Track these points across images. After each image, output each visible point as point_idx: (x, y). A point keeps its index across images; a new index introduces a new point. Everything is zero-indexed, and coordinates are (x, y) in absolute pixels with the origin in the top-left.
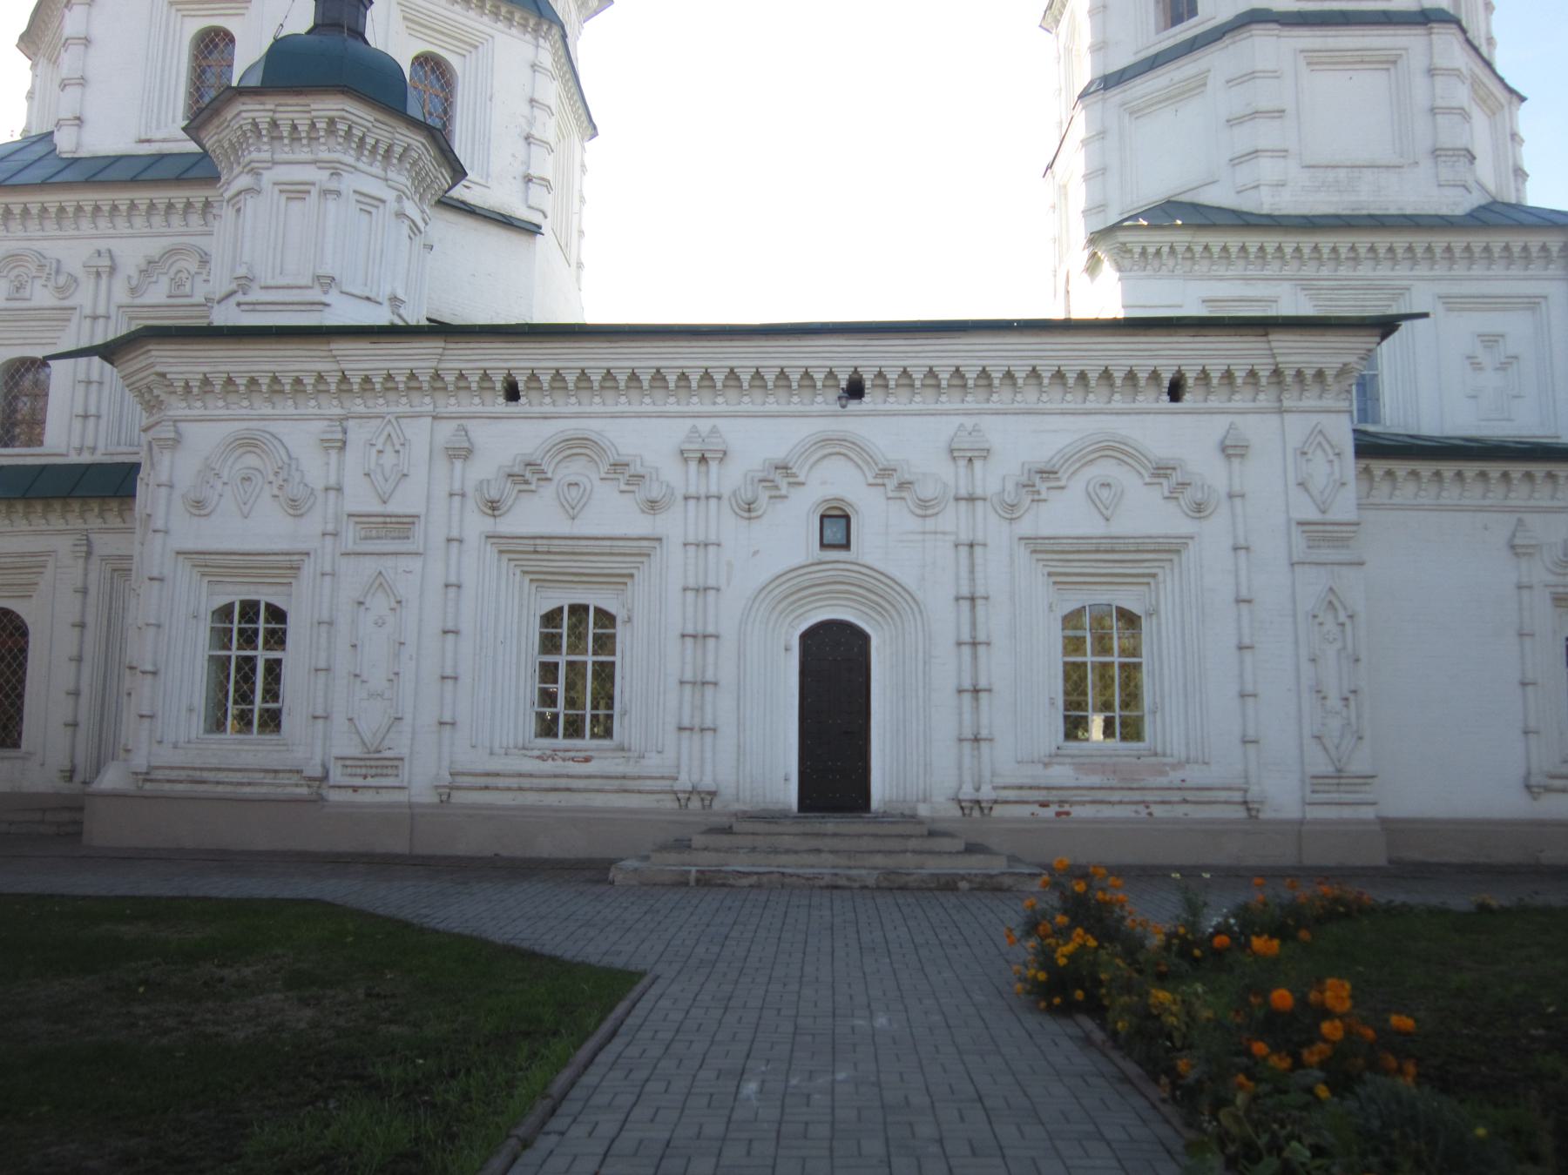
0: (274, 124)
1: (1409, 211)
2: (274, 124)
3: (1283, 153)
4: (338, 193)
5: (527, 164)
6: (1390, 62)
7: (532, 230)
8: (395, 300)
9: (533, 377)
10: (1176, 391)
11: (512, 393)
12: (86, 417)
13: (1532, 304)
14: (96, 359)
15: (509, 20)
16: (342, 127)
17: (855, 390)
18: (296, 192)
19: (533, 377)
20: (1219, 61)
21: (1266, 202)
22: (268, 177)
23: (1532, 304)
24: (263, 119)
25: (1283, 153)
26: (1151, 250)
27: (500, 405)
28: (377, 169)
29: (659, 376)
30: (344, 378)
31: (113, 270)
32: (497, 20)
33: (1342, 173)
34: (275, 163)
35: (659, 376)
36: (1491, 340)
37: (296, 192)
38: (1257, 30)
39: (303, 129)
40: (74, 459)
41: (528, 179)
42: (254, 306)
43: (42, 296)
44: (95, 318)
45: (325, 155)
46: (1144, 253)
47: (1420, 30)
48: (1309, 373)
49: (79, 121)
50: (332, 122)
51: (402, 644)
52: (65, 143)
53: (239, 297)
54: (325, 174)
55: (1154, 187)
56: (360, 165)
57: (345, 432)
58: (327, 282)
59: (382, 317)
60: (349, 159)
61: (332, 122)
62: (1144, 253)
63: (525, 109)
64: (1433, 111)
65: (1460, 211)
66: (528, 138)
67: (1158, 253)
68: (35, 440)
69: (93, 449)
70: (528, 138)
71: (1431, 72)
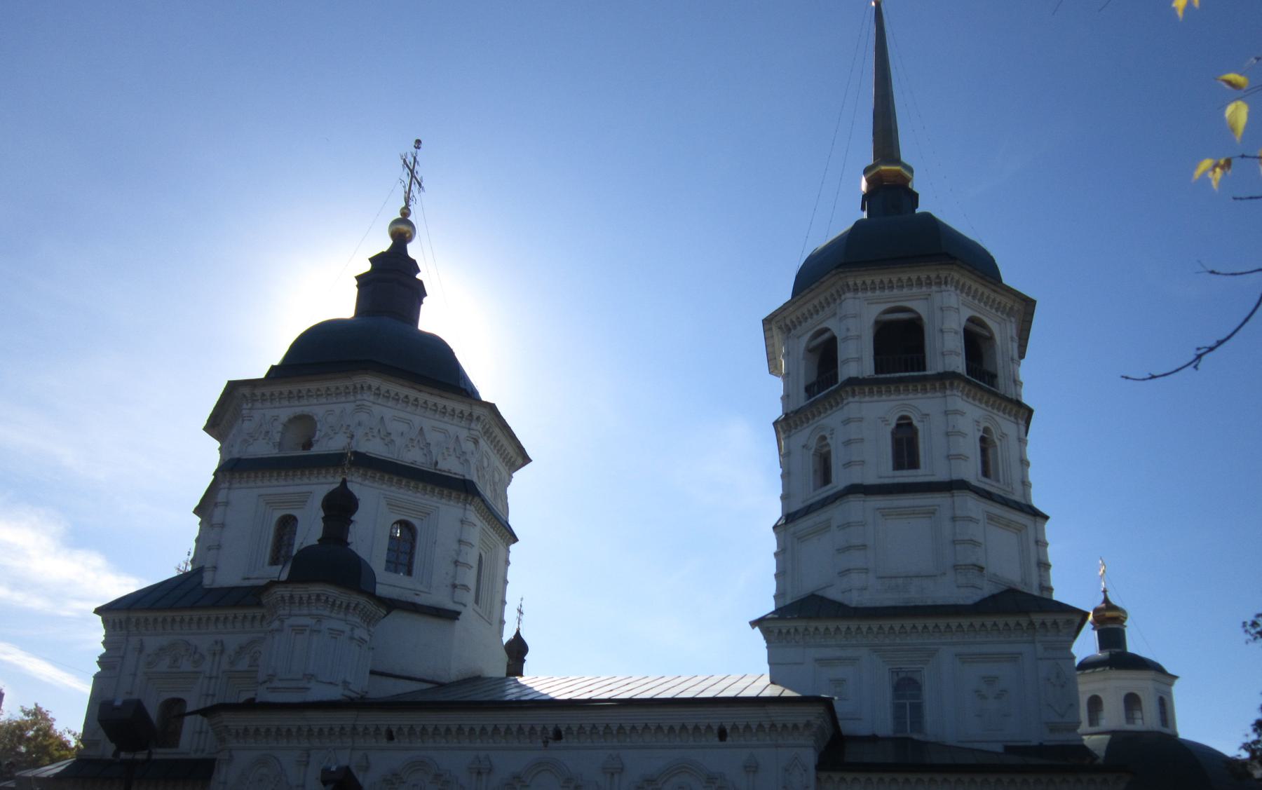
0: (292, 597)
1: (940, 602)
2: (292, 597)
3: (866, 570)
4: (319, 631)
5: (454, 577)
6: (930, 513)
7: (453, 616)
8: (345, 683)
9: (400, 729)
10: (722, 734)
11: (390, 737)
12: (200, 733)
13: (1014, 658)
14: (199, 717)
15: (450, 497)
16: (323, 598)
17: (558, 735)
18: (300, 630)
19: (400, 729)
20: (835, 513)
21: (854, 600)
22: (287, 622)
23: (1014, 658)
24: (287, 594)
25: (866, 570)
26: (784, 631)
27: (384, 742)
28: (342, 615)
29: (460, 729)
30: (310, 730)
31: (222, 652)
32: (442, 497)
33: (900, 581)
34: (290, 615)
35: (460, 729)
36: (990, 680)
37: (300, 630)
38: (851, 497)
39: (305, 599)
40: (193, 756)
41: (454, 586)
42: (274, 689)
43: (186, 665)
44: (210, 678)
45: (315, 612)
46: (780, 632)
47: (948, 495)
48: (790, 725)
49: (215, 568)
50: (318, 596)
51: (786, 770)
52: (207, 580)
53: (268, 685)
54: (314, 621)
55: (808, 586)
56: (333, 615)
57: (309, 756)
58: (310, 677)
59: (335, 694)
60: (326, 613)
61: (318, 596)
62: (780, 632)
63: (455, 546)
64: (954, 542)
65: (970, 602)
66: (456, 563)
67: (788, 632)
68: (175, 744)
69: (203, 750)
70: (456, 563)
71: (954, 519)
